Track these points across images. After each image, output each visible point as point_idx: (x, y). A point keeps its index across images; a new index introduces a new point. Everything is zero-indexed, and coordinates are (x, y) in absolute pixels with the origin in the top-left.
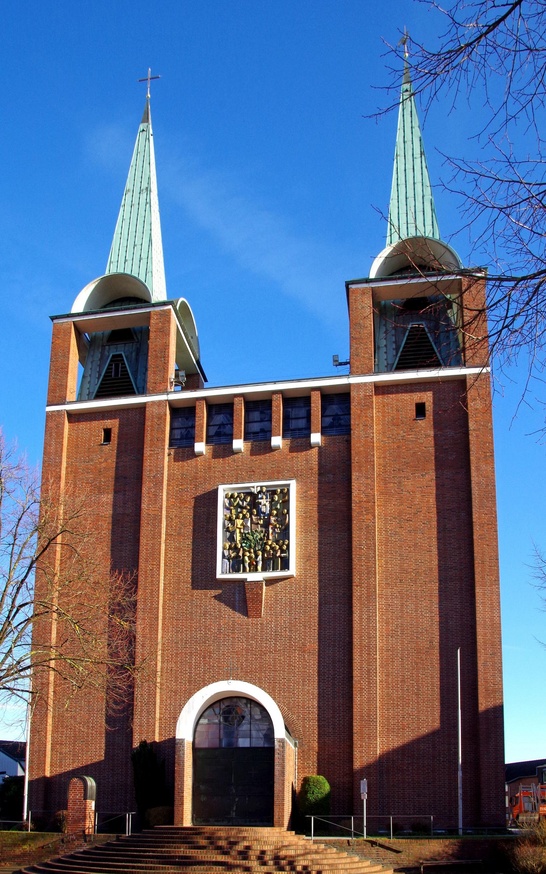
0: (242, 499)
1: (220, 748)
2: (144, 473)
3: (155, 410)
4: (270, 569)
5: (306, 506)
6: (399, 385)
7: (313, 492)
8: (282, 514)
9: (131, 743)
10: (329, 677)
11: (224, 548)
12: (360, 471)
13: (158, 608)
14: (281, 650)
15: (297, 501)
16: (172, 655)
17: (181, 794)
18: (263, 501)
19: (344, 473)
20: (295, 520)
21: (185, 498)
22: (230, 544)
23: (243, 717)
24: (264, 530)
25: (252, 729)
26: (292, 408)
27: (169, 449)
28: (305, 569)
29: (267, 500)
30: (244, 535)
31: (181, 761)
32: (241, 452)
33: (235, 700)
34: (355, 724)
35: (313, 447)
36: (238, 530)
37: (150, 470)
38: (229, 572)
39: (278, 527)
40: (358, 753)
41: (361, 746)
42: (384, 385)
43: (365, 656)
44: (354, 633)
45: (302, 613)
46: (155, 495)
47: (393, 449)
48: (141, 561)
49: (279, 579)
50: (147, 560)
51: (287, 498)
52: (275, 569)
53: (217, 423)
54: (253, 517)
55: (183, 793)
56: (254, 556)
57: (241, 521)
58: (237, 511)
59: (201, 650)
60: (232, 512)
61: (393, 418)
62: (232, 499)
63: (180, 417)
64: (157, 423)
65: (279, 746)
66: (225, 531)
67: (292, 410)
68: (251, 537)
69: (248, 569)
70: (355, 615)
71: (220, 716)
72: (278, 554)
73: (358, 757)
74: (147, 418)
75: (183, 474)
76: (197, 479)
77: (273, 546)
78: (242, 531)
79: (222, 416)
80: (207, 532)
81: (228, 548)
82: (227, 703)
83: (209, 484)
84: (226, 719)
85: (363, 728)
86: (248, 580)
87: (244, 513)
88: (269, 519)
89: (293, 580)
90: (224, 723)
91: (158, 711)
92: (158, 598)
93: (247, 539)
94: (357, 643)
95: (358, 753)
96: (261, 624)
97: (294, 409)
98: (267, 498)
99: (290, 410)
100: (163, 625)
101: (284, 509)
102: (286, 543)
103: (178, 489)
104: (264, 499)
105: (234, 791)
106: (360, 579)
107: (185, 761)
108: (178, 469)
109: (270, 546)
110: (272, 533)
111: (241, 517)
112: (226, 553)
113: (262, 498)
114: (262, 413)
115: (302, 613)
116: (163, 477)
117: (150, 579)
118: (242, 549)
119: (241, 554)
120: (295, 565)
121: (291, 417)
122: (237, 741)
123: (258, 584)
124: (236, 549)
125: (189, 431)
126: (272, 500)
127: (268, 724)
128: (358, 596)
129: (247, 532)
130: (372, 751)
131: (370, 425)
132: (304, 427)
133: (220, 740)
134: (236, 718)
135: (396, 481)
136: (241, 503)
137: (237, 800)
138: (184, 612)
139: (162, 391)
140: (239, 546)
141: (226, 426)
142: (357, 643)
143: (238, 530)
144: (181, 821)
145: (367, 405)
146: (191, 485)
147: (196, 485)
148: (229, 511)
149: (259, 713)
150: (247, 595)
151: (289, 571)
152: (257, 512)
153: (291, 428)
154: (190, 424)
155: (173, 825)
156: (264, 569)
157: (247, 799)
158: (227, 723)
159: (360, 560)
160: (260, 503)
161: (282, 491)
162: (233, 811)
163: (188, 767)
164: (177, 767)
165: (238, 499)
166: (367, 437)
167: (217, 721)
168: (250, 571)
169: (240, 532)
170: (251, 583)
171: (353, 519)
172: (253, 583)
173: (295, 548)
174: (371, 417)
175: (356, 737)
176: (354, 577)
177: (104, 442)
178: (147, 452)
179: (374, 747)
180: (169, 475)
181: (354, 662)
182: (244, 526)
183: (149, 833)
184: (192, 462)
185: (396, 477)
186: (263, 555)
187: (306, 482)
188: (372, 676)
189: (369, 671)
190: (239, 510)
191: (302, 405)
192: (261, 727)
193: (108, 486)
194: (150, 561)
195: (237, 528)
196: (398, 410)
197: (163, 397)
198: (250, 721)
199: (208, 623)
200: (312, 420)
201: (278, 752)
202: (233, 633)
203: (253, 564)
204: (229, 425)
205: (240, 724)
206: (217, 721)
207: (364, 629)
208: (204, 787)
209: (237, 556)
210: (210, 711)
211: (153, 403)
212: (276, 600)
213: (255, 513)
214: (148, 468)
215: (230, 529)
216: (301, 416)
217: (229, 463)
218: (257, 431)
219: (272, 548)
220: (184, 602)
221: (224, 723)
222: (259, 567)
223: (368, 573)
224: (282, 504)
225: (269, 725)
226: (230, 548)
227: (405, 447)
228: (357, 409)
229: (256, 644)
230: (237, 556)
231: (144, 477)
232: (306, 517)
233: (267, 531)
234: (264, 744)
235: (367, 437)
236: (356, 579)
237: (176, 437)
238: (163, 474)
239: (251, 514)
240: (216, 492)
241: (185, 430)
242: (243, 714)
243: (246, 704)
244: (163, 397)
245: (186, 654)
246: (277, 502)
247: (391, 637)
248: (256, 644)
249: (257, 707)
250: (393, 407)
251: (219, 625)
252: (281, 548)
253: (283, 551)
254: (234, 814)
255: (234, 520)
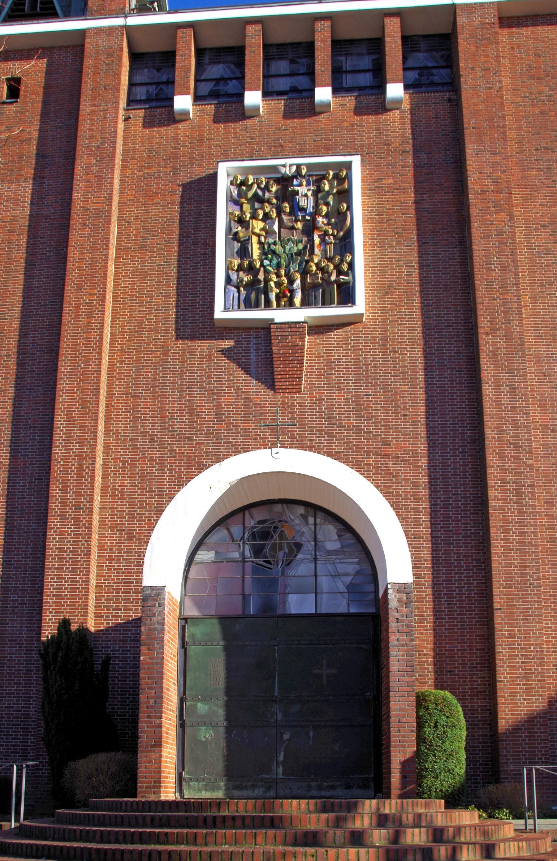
0: (263, 186)
1: (244, 616)
2: (80, 142)
3: (103, 42)
4: (318, 304)
5: (380, 203)
6: (539, 15)
7: (391, 181)
8: (336, 214)
9: (39, 633)
10: (437, 505)
11: (228, 268)
12: (480, 141)
13: (99, 372)
14: (340, 452)
15: (363, 195)
16: (124, 463)
17: (155, 721)
18: (303, 190)
19: (448, 152)
20: (362, 225)
21: (154, 188)
22: (239, 261)
23: (299, 546)
24: (305, 239)
25: (318, 573)
26: (347, 55)
27: (126, 110)
28: (383, 309)
29: (309, 187)
30: (266, 247)
31: (155, 639)
32: (258, 115)
33: (278, 508)
34: (496, 591)
35: (390, 110)
36: (255, 239)
37: (91, 137)
38: (239, 307)
39: (331, 233)
40: (505, 649)
41: (511, 635)
42: (512, 15)
43: (510, 461)
44: (486, 418)
45: (379, 385)
46: (100, 178)
47: (533, 115)
48: (68, 288)
49: (333, 326)
50: (79, 288)
51: (346, 185)
52: (326, 302)
53: (214, 77)
54: (285, 218)
55: (161, 717)
56: (286, 281)
57: (261, 225)
58: (253, 207)
59: (183, 453)
60: (244, 209)
61: (530, 68)
62: (244, 188)
63: (146, 67)
64: (104, 62)
65: (400, 601)
66: (232, 239)
67: (346, 59)
68: (279, 249)
69: (275, 304)
70: (485, 386)
71: (244, 543)
72: (333, 278)
73: (505, 656)
74: (86, 54)
75: (150, 151)
76: (176, 158)
77: (323, 264)
78: (263, 239)
79: (221, 66)
80: (195, 244)
81: (236, 267)
82: (260, 514)
83: (200, 166)
84: (258, 551)
85: (513, 598)
86: (276, 321)
87: (267, 210)
88: (314, 220)
89: (360, 327)
90: (253, 559)
91: (93, 569)
92: (100, 353)
93: (274, 252)
94: (492, 438)
95: (505, 649)
96: (301, 405)
97: (349, 58)
98: (308, 184)
99: (343, 58)
100: (107, 407)
101: (340, 202)
102: (348, 259)
103: (141, 173)
104: (304, 187)
105: (280, 716)
106: (491, 322)
107: (165, 641)
108: (143, 143)
109: (317, 265)
110: (320, 244)
111: (261, 217)
112: (234, 276)
113: (300, 185)
114: (292, 62)
115: (379, 385)
116: (114, 148)
117: (84, 321)
118: (262, 269)
119: (261, 276)
120: (364, 300)
121: (344, 69)
122: (285, 602)
123: (296, 328)
124: (251, 269)
125: (161, 89)
126: (318, 190)
127: (356, 560)
128: (490, 351)
129: (272, 241)
130: (532, 644)
131: (493, 69)
132: (368, 85)
133: (245, 597)
134: (281, 548)
135: (542, 167)
136: (260, 193)
137: (286, 737)
138: (150, 384)
139: (115, 12)
140: (258, 265)
141: (229, 81)
142: (492, 438)
143: (255, 239)
144: (154, 787)
145: (487, 39)
146: (166, 167)
147: (174, 168)
148: (238, 207)
149: (336, 537)
150: (274, 348)
151: (354, 308)
152: (291, 208)
153: (344, 86)
154: (164, 78)
155: (136, 797)
156: (305, 303)
157: (311, 734)
158: (260, 561)
159: (489, 287)
160: (297, 193)
161: (336, 176)
162: (278, 764)
163: (171, 658)
164: (145, 654)
165: (255, 187)
166: (490, 88)
167: (236, 555)
168: (278, 306)
169: (260, 243)
170: (283, 326)
171: (473, 219)
172: (287, 326)
173: (363, 272)
174: (495, 57)
175: (499, 617)
176: (480, 319)
177: (7, 99)
178: (85, 108)
179: (537, 637)
180: (125, 152)
181: (488, 472)
182: (268, 232)
183: (74, 820)
184: (169, 131)
185: (542, 160)
186: (303, 281)
187: (379, 165)
188: (525, 499)
189: (518, 489)
190: (257, 205)
191: (365, 52)
192: (341, 568)
193: (12, 170)
194: (86, 289)
195: (254, 233)
196: (537, 55)
197: (118, 22)
198: (315, 555)
199: (196, 401)
200: (387, 62)
201: (397, 615)
202: (245, 422)
203: (285, 296)
204: (234, 81)
205: (291, 561)
206: (236, 555)
207: (505, 411)
208: (207, 707)
209: (255, 282)
210: (221, 534)
211: (99, 30)
212: (329, 362)
213: (288, 210)
214: (88, 134)
215: (241, 235)
216: (362, 68)
217: (235, 133)
218: (285, 89)
219: (323, 270)
220: (150, 366)
221: (253, 559)
222: (297, 300)
223: (506, 313)
224: (337, 195)
225: (358, 563)
226: (240, 268)
227: (554, 113)
228: (469, 44)
229: (291, 441)
230: (255, 282)
231: (79, 148)
232: (381, 222)
233: (311, 241)
234: (348, 606)
235: (490, 88)
236: (484, 322)
237: (138, 98)
238: (115, 143)
239: (280, 211)
240: (213, 178)
241: (154, 87)
242: (298, 540)
243: (304, 517)
244: (118, 22)
245: (151, 459)
246: (328, 193)
247: (552, 432)
248: (291, 441)
249: (330, 523)
250: (529, 49)
251: (219, 406)
252: (338, 268)
253: (340, 273)
254: (281, 770)
255: (249, 221)
